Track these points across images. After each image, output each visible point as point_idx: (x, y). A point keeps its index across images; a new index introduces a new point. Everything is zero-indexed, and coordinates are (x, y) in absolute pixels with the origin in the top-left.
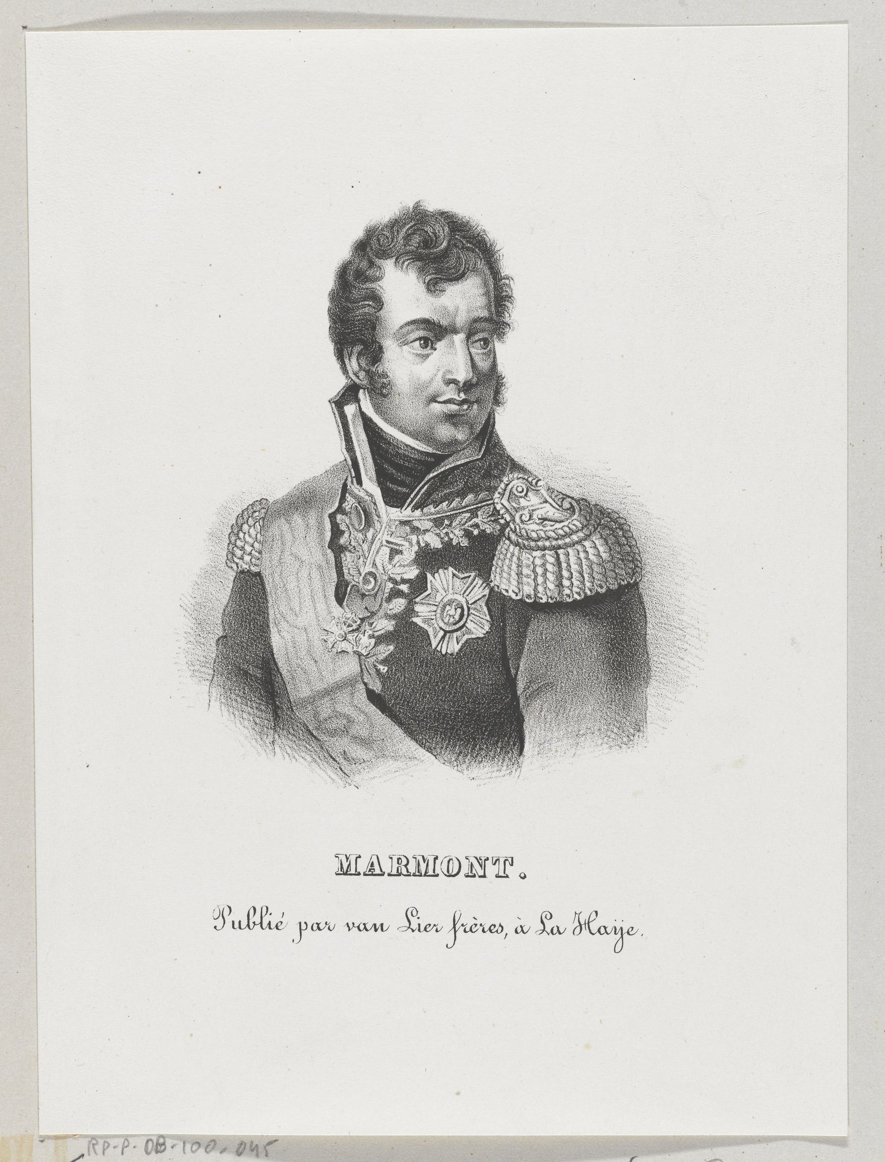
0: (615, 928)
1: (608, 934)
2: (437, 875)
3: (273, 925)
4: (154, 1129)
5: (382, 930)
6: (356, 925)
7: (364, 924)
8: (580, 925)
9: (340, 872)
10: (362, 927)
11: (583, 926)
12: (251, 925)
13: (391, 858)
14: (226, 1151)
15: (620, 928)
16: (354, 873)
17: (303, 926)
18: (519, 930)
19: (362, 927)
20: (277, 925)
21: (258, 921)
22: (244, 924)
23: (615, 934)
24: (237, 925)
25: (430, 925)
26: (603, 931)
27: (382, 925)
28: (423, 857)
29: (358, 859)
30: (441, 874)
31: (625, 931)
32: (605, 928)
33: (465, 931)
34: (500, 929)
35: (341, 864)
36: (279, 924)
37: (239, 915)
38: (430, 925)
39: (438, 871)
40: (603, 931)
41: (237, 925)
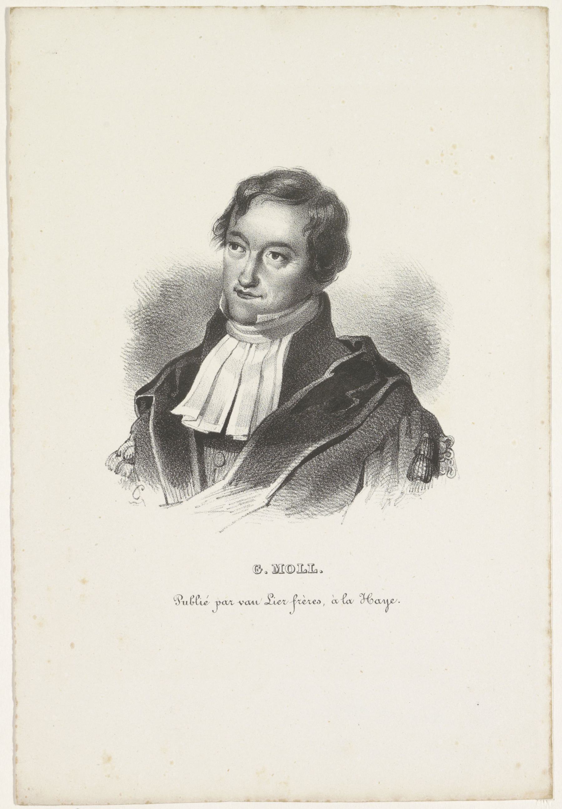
0: (384, 600)
1: (380, 603)
2: (284, 573)
3: (202, 603)
4: (474, 5)
5: (257, 604)
6: (245, 602)
7: (350, 600)
8: (364, 599)
9: (274, 572)
10: (247, 603)
11: (367, 598)
12: (192, 603)
13: (298, 565)
14: (296, 208)
15: (252, 601)
16: (301, 572)
17: (218, 603)
18: (334, 602)
19: (377, 602)
20: (303, 602)
21: (195, 601)
22: (189, 603)
23: (385, 603)
24: (185, 603)
25: (280, 601)
26: (378, 602)
27: (256, 602)
28: (277, 565)
29: (302, 566)
30: (285, 572)
31: (389, 602)
32: (379, 600)
33: (309, 603)
34: (319, 602)
35: (275, 569)
36: (392, 600)
37: (186, 598)
38: (280, 601)
39: (284, 570)
40: (378, 602)
41: (185, 603)
